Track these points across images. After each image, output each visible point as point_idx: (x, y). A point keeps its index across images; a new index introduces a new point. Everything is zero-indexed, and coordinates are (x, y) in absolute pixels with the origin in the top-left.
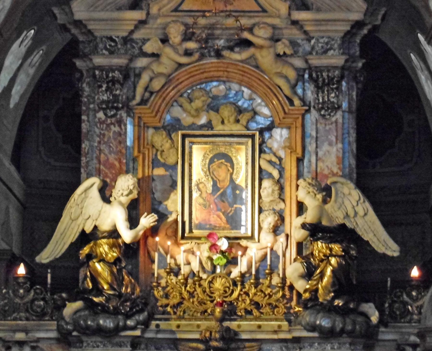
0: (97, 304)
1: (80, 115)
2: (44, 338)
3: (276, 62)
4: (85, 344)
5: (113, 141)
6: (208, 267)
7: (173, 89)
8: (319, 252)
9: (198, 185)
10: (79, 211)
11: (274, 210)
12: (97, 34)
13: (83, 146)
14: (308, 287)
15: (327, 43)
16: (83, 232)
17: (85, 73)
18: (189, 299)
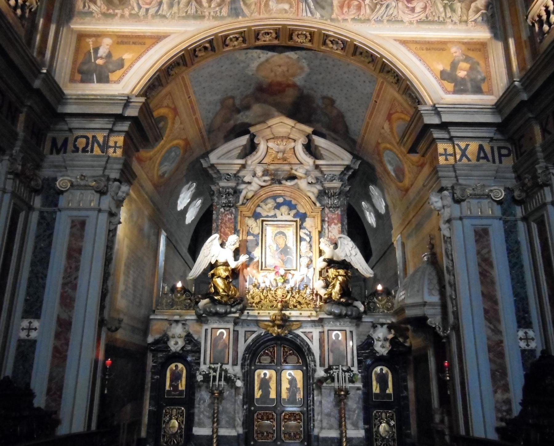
0: (216, 300)
1: (212, 211)
2: (189, 319)
4: (209, 321)
6: (274, 284)
8: (332, 274)
9: (269, 246)
10: (209, 252)
11: (307, 256)
12: (221, 172)
13: (213, 225)
14: (326, 292)
15: (333, 177)
16: (210, 263)
18: (264, 299)
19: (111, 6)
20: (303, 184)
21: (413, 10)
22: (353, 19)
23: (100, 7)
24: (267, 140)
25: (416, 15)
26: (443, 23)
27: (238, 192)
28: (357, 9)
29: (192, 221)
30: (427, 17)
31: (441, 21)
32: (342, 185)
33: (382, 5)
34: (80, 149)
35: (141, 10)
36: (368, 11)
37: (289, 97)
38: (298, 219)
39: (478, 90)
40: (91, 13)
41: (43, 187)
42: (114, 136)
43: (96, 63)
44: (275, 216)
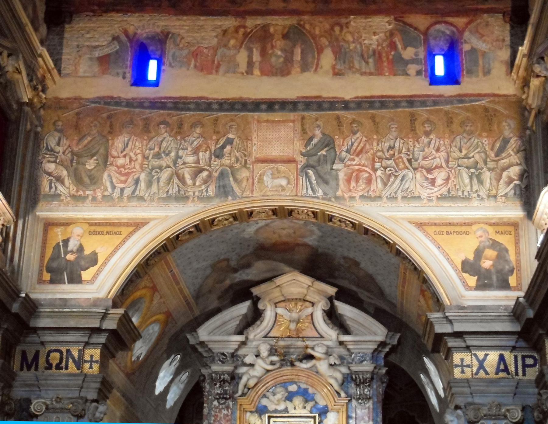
1: (203, 404)
3: (329, 368)
5: (223, 419)
7: (263, 386)
12: (214, 351)
15: (362, 357)
17: (207, 376)
19: (80, 187)
20: (323, 366)
21: (433, 182)
22: (362, 197)
23: (68, 188)
24: (276, 304)
25: (436, 189)
26: (467, 199)
27: (236, 377)
28: (366, 183)
29: (176, 403)
30: (449, 192)
31: (466, 196)
32: (375, 368)
33: (396, 176)
34: (54, 365)
35: (116, 191)
36: (380, 185)
37: (301, 255)
38: (317, 415)
39: (504, 285)
40: (59, 195)
41: (15, 410)
42: (90, 349)
43: (66, 260)
44: (286, 410)
